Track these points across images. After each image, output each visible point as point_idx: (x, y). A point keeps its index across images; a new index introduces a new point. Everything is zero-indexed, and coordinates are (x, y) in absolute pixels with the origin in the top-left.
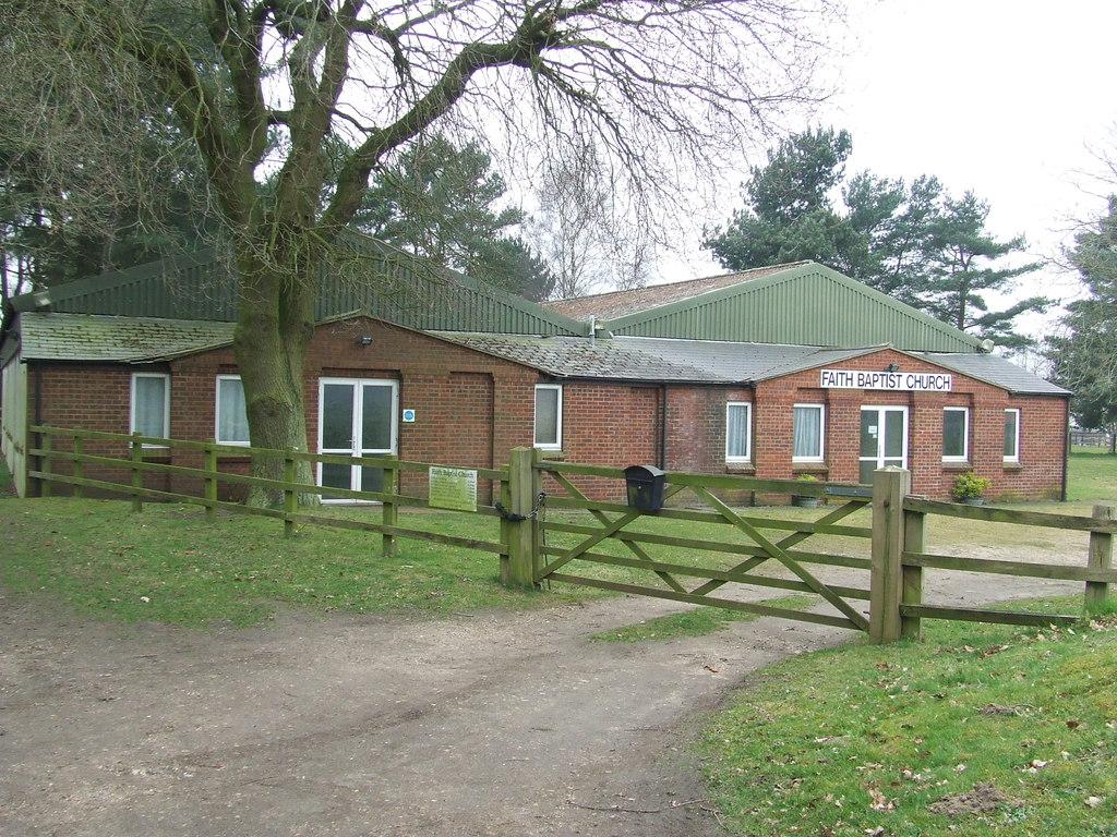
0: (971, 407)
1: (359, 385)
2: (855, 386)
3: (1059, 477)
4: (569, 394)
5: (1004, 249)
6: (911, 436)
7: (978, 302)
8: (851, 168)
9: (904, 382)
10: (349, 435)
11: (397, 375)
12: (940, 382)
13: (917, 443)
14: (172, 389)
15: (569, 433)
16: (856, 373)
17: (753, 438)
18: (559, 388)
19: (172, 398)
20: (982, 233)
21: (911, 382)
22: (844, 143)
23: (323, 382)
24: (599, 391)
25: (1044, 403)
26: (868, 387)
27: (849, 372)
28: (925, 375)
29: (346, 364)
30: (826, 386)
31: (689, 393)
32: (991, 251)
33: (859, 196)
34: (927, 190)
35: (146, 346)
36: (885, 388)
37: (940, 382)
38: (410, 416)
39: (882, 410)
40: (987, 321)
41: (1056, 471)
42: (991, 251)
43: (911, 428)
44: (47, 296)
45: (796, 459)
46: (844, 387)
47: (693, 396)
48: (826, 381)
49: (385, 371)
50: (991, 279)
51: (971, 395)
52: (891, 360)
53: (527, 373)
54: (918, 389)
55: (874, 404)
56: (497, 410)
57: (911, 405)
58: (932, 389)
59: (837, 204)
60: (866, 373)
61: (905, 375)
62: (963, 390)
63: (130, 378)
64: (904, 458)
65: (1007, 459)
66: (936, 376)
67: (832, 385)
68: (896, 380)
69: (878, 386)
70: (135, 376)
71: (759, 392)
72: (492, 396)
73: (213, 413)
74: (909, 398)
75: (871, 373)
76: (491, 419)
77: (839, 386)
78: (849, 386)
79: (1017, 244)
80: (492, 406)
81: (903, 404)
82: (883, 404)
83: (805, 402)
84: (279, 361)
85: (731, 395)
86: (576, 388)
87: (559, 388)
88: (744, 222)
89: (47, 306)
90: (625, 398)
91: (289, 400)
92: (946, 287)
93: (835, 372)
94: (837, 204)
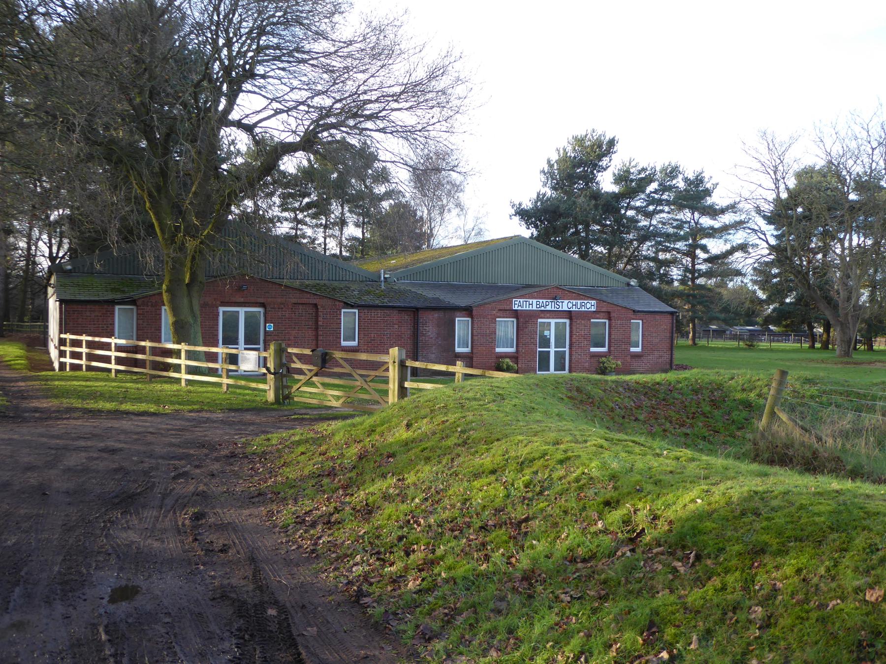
0: (610, 319)
1: (242, 311)
2: (535, 308)
3: (668, 360)
4: (362, 315)
5: (723, 211)
6: (571, 336)
7: (704, 249)
8: (615, 163)
9: (565, 305)
10: (237, 338)
11: (263, 305)
12: (589, 306)
13: (574, 340)
14: (138, 314)
15: (362, 336)
16: (535, 301)
17: (472, 338)
18: (356, 311)
19: (138, 319)
20: (709, 201)
21: (570, 305)
22: (612, 143)
23: (222, 309)
24: (380, 312)
25: (658, 317)
26: (543, 308)
27: (531, 301)
28: (579, 302)
29: (234, 299)
30: (516, 308)
31: (433, 313)
32: (713, 212)
33: (622, 178)
34: (672, 172)
35: (123, 292)
36: (553, 309)
37: (589, 306)
38: (270, 327)
39: (553, 322)
40: (712, 260)
41: (668, 356)
42: (713, 212)
43: (571, 332)
44: (231, 213)
45: (498, 350)
46: (527, 308)
47: (436, 315)
48: (516, 306)
49: (257, 303)
50: (712, 233)
51: (609, 313)
52: (556, 294)
53: (337, 303)
54: (574, 309)
55: (548, 318)
56: (320, 323)
57: (571, 319)
58: (583, 309)
59: (606, 183)
60: (541, 301)
61: (566, 301)
62: (604, 310)
63: (114, 309)
64: (567, 349)
65: (633, 349)
66: (586, 302)
67: (520, 308)
68: (560, 304)
69: (549, 308)
70: (117, 307)
71: (474, 313)
72: (317, 316)
73: (161, 327)
74: (569, 314)
75: (544, 301)
76: (317, 329)
77: (524, 308)
78: (531, 308)
79: (732, 207)
80: (317, 321)
81: (566, 318)
82: (553, 318)
83: (504, 317)
84: (185, 301)
85: (458, 314)
86: (366, 311)
87: (356, 311)
88: (540, 197)
89: (70, 270)
90: (395, 316)
91: (191, 321)
92: (684, 238)
93: (521, 300)
94: (606, 183)
